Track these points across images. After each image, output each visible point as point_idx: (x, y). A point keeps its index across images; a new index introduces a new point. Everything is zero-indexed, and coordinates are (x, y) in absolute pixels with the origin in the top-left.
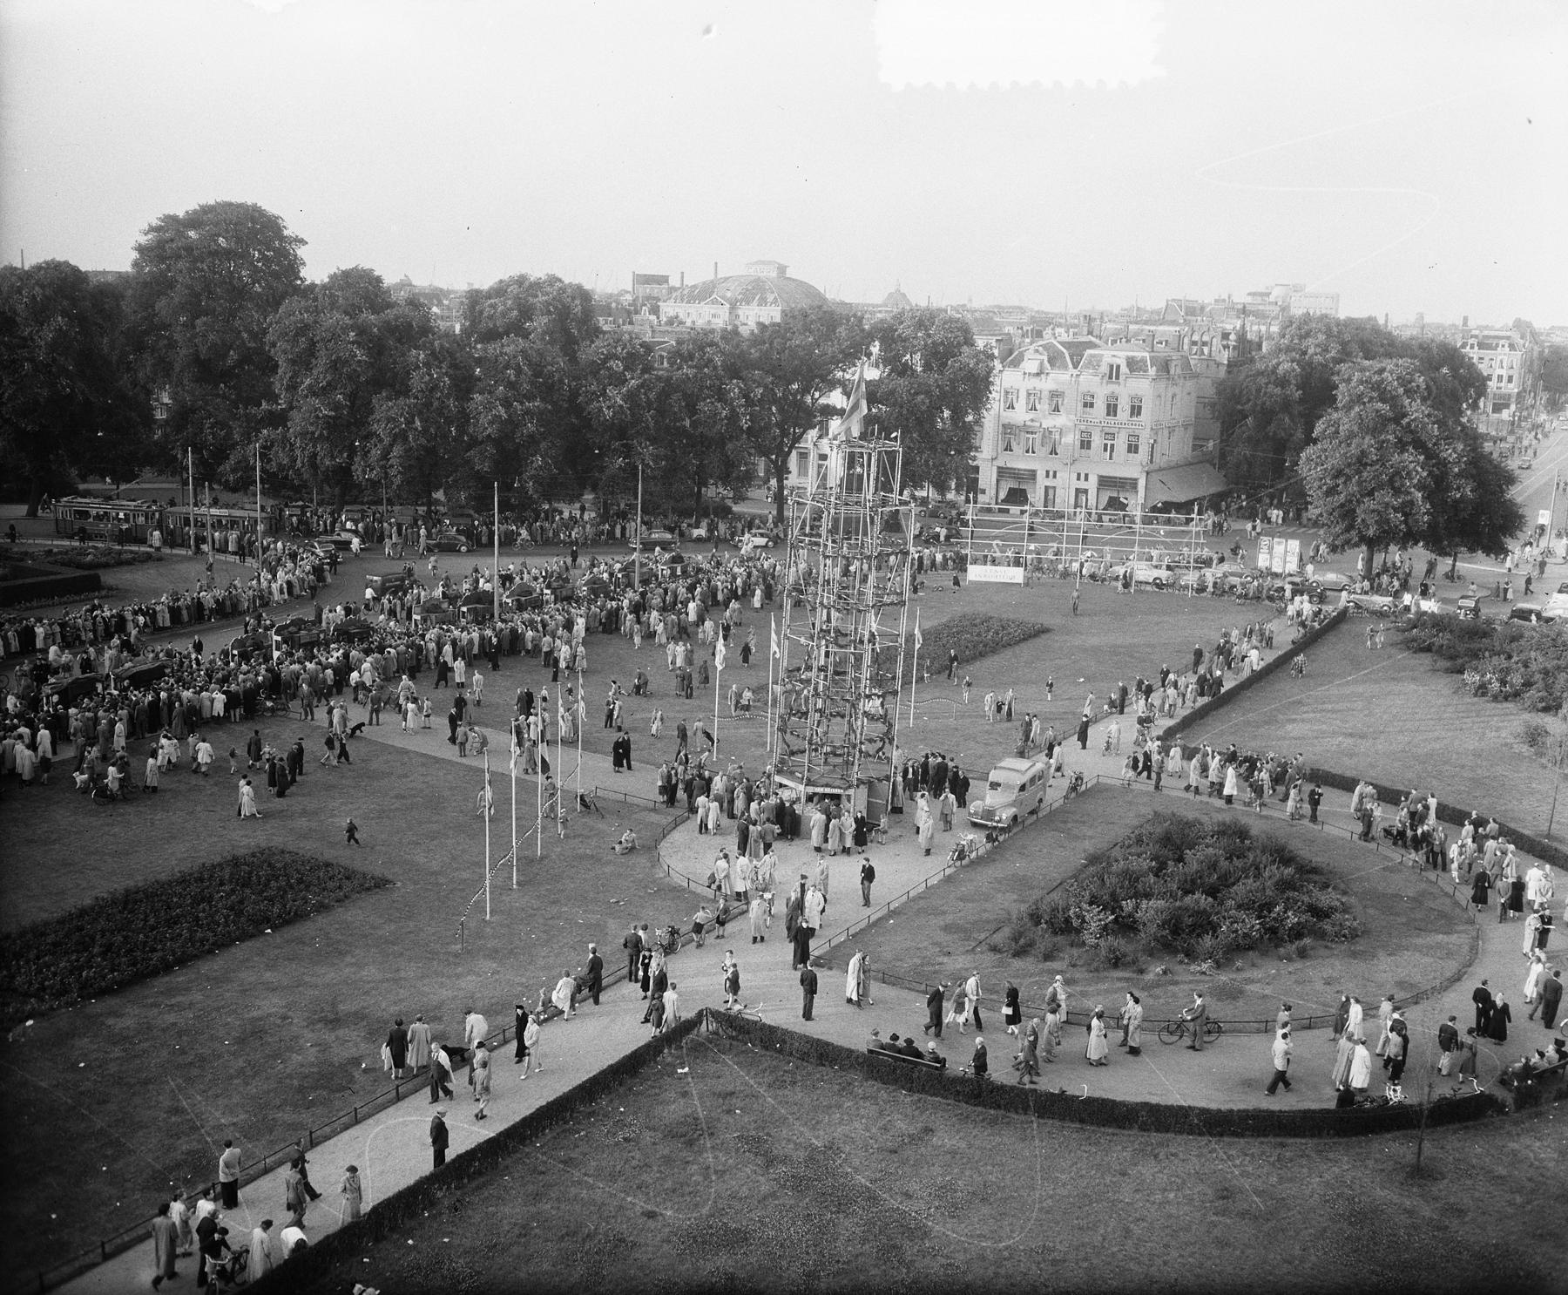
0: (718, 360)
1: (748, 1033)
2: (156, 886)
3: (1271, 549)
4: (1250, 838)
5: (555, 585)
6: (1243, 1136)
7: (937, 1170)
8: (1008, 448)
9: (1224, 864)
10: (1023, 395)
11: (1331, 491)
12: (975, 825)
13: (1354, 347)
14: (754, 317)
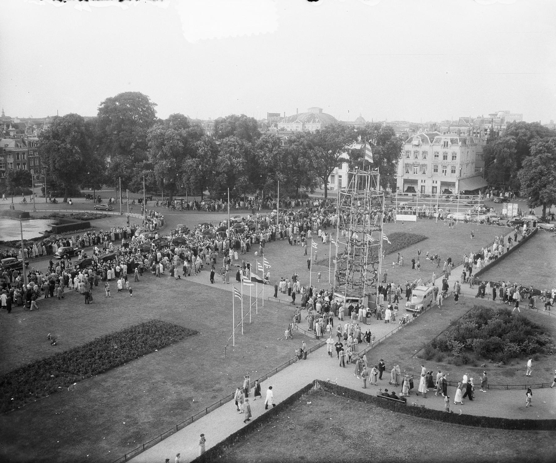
0: (305, 142)
1: (332, 389)
2: (116, 334)
3: (507, 207)
4: (512, 315)
5: (249, 224)
6: (521, 429)
7: (407, 441)
8: (407, 172)
9: (503, 325)
10: (412, 153)
11: (529, 186)
12: (408, 310)
13: (535, 133)
14: (313, 128)
